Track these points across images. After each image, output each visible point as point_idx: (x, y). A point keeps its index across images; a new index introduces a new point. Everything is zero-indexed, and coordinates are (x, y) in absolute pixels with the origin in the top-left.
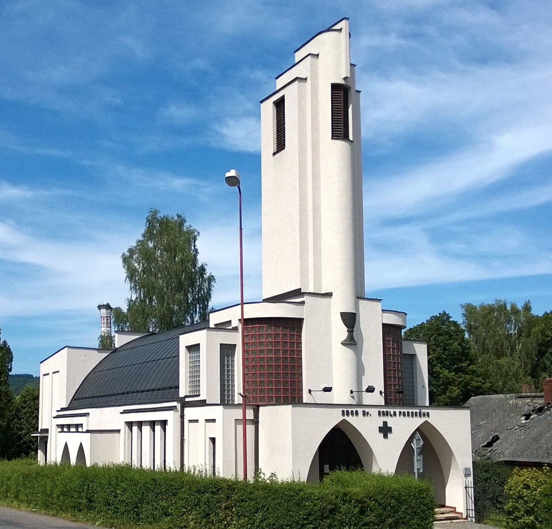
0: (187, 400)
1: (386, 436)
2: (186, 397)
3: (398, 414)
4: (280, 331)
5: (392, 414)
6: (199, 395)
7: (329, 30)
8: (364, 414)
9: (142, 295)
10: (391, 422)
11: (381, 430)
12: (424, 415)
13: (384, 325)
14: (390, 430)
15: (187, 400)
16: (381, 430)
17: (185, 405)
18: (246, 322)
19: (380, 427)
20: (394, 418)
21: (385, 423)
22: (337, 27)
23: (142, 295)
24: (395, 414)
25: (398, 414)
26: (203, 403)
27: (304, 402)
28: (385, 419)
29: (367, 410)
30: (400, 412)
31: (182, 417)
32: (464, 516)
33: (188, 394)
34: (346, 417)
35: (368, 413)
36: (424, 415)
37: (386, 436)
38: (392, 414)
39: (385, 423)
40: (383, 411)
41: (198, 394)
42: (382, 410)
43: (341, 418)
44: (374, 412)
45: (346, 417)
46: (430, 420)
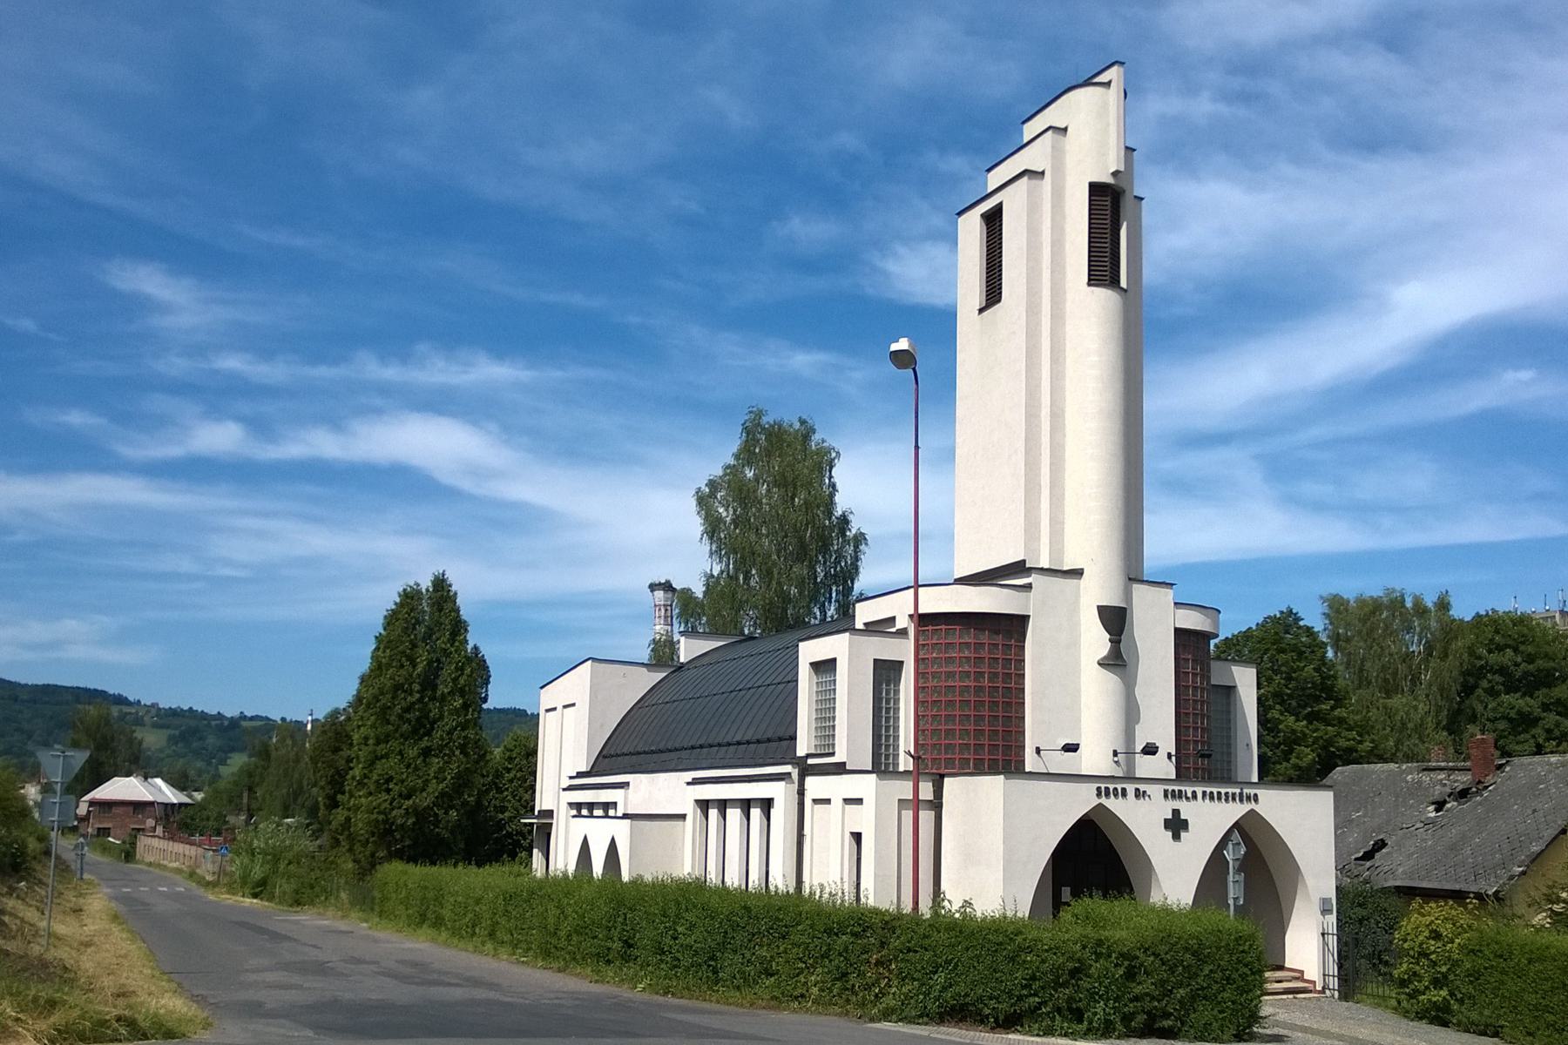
0: (810, 761)
1: (1176, 837)
2: (808, 756)
3: (1200, 795)
4: (985, 638)
6: (833, 754)
7: (1088, 83)
8: (1139, 794)
10: (1187, 810)
11: (1168, 824)
12: (1249, 798)
13: (1177, 630)
15: (810, 761)
16: (1168, 824)
17: (806, 770)
18: (924, 621)
20: (1193, 803)
21: (1176, 812)
22: (1102, 78)
25: (1200, 795)
26: (840, 769)
28: (1177, 804)
29: (1142, 787)
30: (1204, 793)
31: (801, 792)
33: (813, 751)
34: (1103, 800)
36: (1249, 798)
37: (1176, 837)
39: (1176, 812)
43: (1095, 802)
44: (1156, 791)
45: (1103, 800)
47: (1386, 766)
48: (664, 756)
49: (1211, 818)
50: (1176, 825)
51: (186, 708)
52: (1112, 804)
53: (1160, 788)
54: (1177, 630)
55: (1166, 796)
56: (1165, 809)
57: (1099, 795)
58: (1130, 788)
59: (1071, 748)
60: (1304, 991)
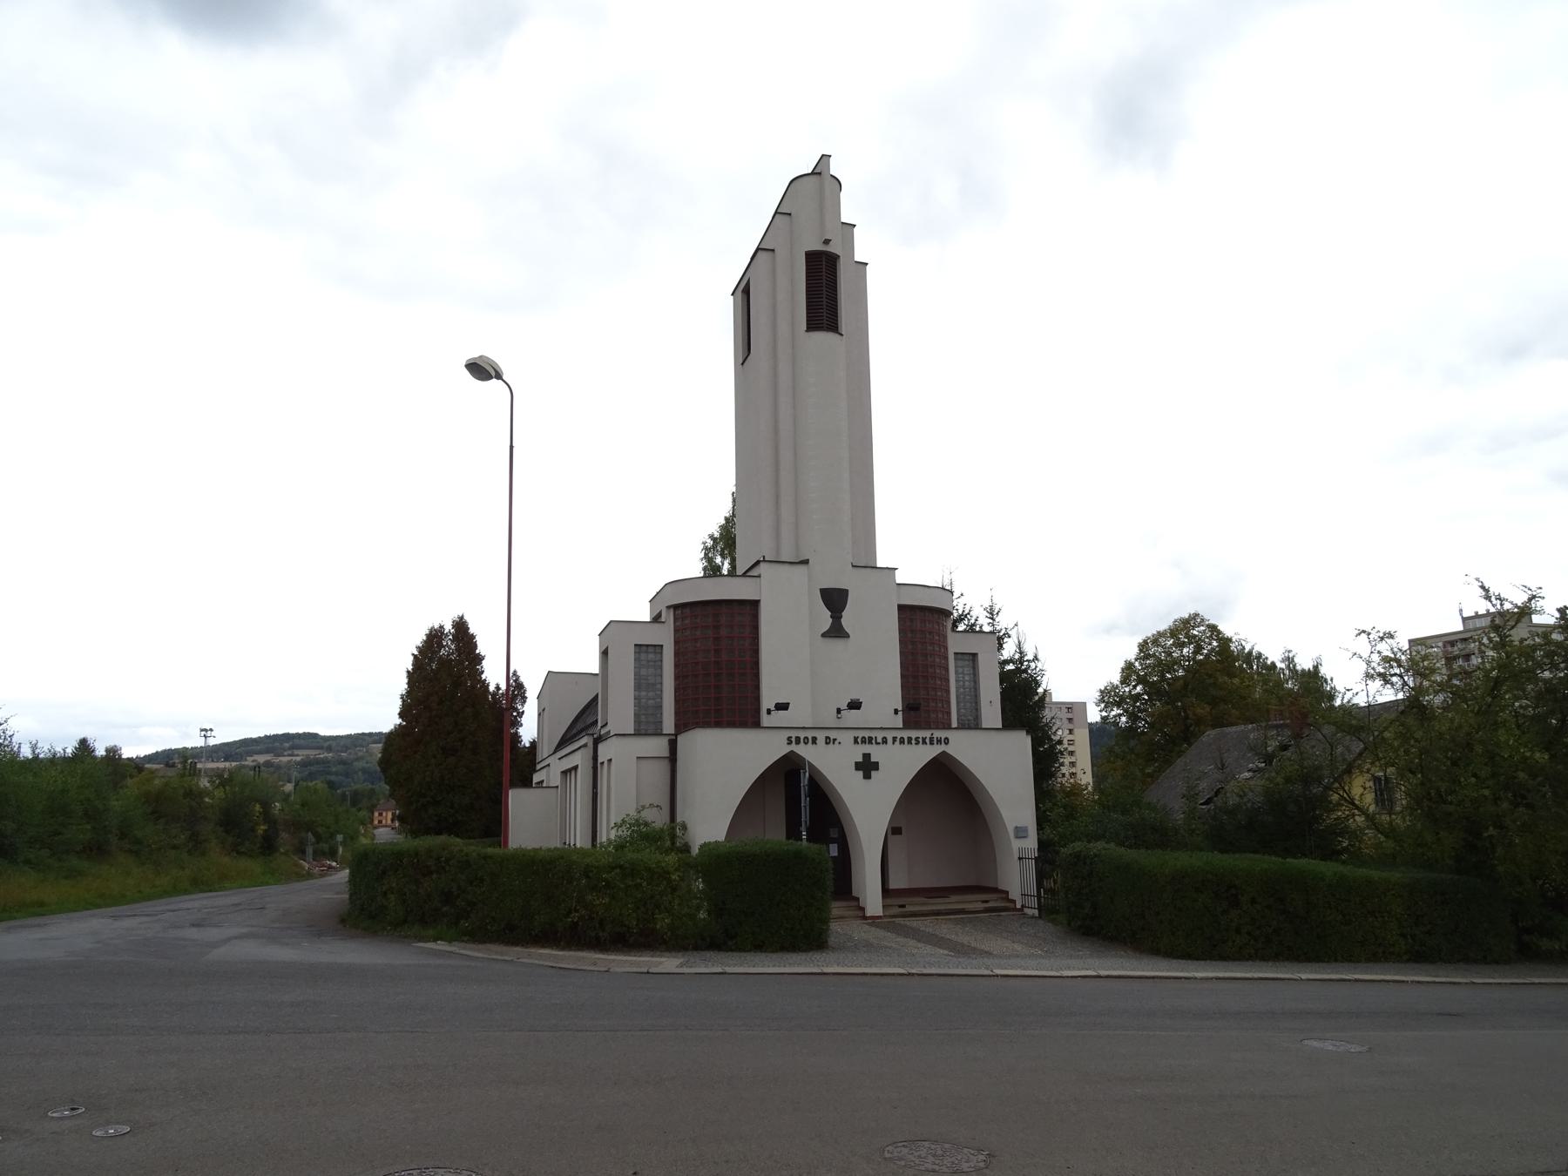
1: (867, 776)
3: (890, 740)
8: (828, 741)
10: (877, 753)
11: (858, 766)
12: (939, 741)
13: (901, 608)
14: (876, 766)
21: (867, 756)
24: (814, 740)
25: (890, 740)
28: (867, 748)
29: (832, 734)
30: (894, 739)
34: (793, 747)
36: (939, 741)
37: (867, 776)
39: (867, 756)
43: (786, 749)
45: (793, 747)
46: (950, 749)
47: (1234, 729)
48: (953, 902)
49: (903, 762)
50: (867, 767)
51: (471, 631)
52: (801, 750)
53: (851, 735)
54: (901, 608)
55: (856, 741)
56: (857, 754)
57: (790, 742)
58: (821, 736)
59: (855, 705)
60: (1005, 909)
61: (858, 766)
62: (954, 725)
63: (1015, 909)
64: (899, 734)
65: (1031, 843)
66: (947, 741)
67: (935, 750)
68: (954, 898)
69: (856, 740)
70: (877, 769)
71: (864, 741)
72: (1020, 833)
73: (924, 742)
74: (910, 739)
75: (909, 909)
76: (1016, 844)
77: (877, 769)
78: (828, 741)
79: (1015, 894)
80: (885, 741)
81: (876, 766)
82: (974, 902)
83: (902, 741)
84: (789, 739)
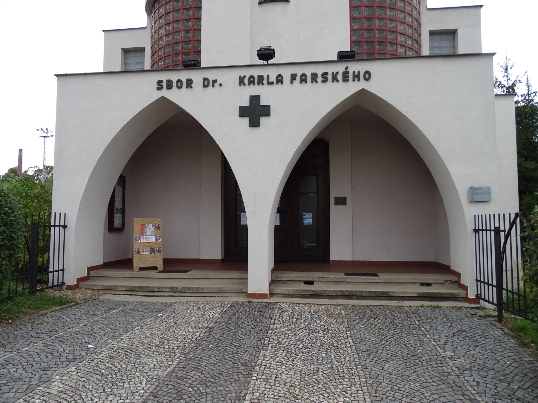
3: (287, 79)
5: (273, 79)
8: (206, 83)
9: (65, 306)
10: (267, 95)
11: (243, 112)
12: (356, 77)
14: (266, 111)
19: (241, 108)
20: (276, 88)
21: (255, 99)
23: (65, 306)
24: (189, 83)
25: (287, 79)
27: (202, 66)
28: (255, 90)
29: (211, 75)
30: (293, 77)
32: (472, 295)
35: (215, 81)
36: (356, 77)
38: (273, 79)
39: (255, 99)
40: (304, 75)
41: (372, 52)
42: (248, 73)
43: (158, 95)
44: (230, 79)
45: (165, 93)
46: (372, 87)
53: (237, 74)
61: (243, 112)
62: (426, 51)
63: (466, 299)
64: (256, 72)
65: (506, 201)
66: (368, 76)
67: (351, 88)
68: (383, 277)
69: (241, 81)
70: (268, 115)
71: (252, 81)
72: (479, 195)
73: (335, 78)
74: (314, 77)
75: (316, 287)
76: (470, 212)
77: (268, 115)
78: (206, 83)
79: (468, 278)
80: (280, 80)
81: (266, 111)
82: (409, 284)
83: (303, 79)
84: (160, 83)
